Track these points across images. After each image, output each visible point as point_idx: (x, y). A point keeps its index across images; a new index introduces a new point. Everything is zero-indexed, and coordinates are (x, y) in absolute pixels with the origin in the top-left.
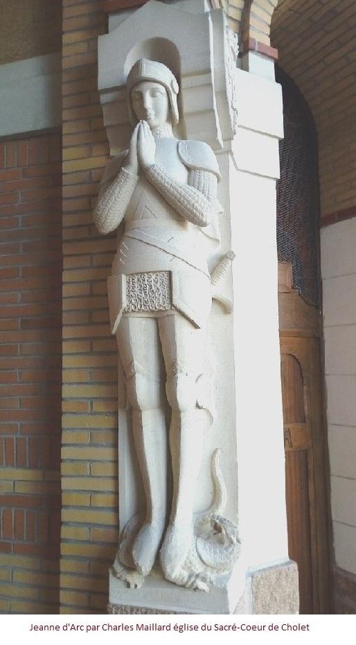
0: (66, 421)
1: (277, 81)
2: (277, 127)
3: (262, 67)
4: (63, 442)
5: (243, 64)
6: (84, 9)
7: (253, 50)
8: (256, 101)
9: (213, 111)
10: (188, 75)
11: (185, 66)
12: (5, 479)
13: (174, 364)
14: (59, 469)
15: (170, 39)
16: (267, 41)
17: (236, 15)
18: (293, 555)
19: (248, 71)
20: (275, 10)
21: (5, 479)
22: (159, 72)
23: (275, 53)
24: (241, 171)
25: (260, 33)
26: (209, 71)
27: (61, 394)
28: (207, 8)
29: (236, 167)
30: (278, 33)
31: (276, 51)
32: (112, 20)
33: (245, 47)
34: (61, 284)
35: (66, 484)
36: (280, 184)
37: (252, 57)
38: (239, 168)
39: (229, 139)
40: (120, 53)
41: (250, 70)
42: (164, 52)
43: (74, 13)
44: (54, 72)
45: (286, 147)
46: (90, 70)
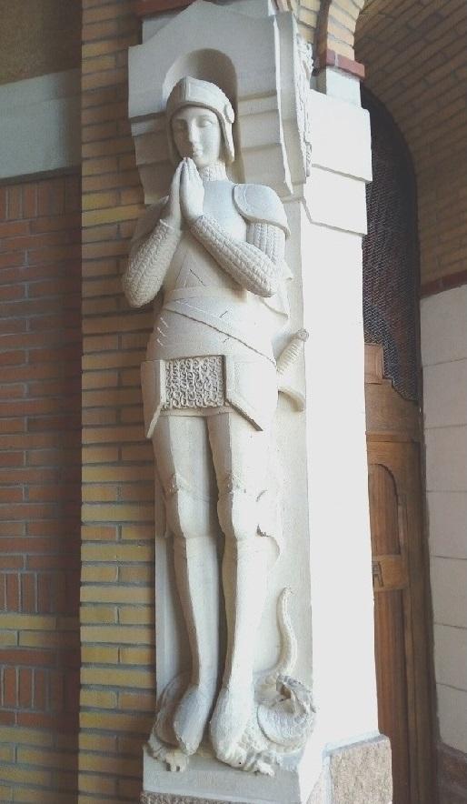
0: (87, 553)
1: (364, 106)
2: (364, 167)
3: (344, 88)
4: (82, 580)
5: (319, 84)
6: (110, 12)
7: (332, 65)
8: (336, 133)
9: (280, 145)
10: (247, 98)
11: (242, 87)
12: (7, 628)
13: (228, 478)
14: (77, 615)
15: (223, 51)
16: (351, 54)
17: (310, 19)
18: (385, 727)
19: (325, 93)
20: (361, 13)
21: (7, 628)
22: (209, 94)
23: (360, 69)
24: (316, 224)
25: (341, 43)
26: (274, 93)
27: (80, 517)
28: (272, 11)
29: (310, 220)
30: (364, 44)
31: (362, 67)
32: (148, 26)
33: (321, 62)
34: (80, 372)
35: (86, 634)
36: (367, 241)
37: (331, 75)
38: (314, 220)
39: (300, 181)
40: (157, 70)
41: (328, 92)
42: (215, 68)
43: (97, 17)
44: (71, 95)
45: (375, 193)
46: (118, 91)
